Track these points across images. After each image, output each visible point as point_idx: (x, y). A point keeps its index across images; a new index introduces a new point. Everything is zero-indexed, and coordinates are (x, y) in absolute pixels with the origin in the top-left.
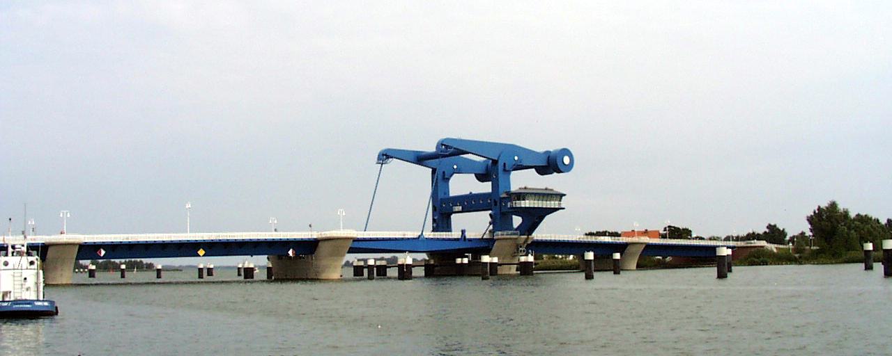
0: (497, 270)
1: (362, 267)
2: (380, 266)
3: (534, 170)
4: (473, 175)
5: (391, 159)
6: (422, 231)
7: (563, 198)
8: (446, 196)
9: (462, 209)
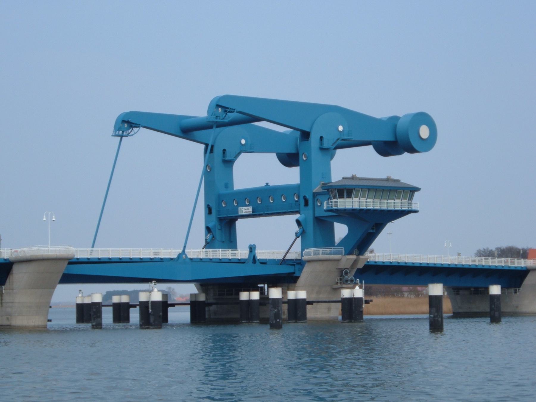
0: (361, 313)
3: (370, 148)
4: (274, 155)
5: (135, 129)
6: (185, 247)
7: (416, 193)
8: (229, 191)
9: (253, 211)
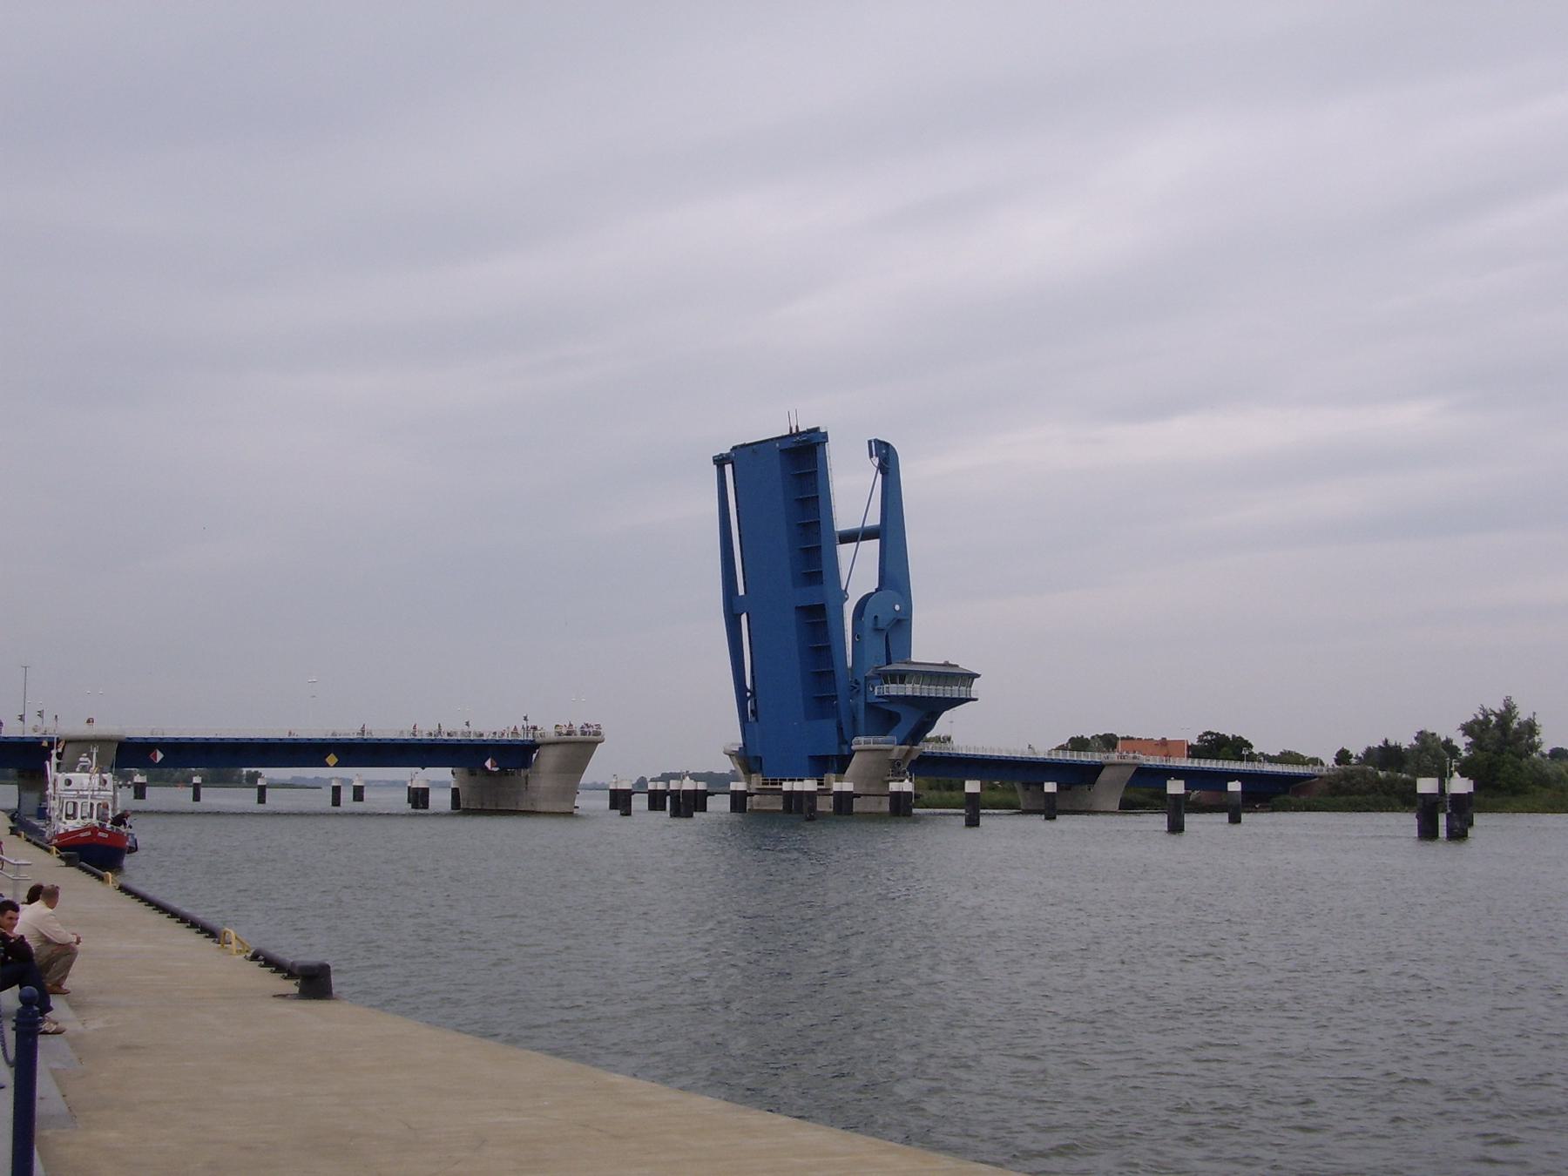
1: (664, 793)
2: (841, 792)
7: (976, 680)
